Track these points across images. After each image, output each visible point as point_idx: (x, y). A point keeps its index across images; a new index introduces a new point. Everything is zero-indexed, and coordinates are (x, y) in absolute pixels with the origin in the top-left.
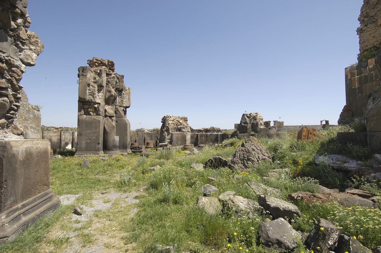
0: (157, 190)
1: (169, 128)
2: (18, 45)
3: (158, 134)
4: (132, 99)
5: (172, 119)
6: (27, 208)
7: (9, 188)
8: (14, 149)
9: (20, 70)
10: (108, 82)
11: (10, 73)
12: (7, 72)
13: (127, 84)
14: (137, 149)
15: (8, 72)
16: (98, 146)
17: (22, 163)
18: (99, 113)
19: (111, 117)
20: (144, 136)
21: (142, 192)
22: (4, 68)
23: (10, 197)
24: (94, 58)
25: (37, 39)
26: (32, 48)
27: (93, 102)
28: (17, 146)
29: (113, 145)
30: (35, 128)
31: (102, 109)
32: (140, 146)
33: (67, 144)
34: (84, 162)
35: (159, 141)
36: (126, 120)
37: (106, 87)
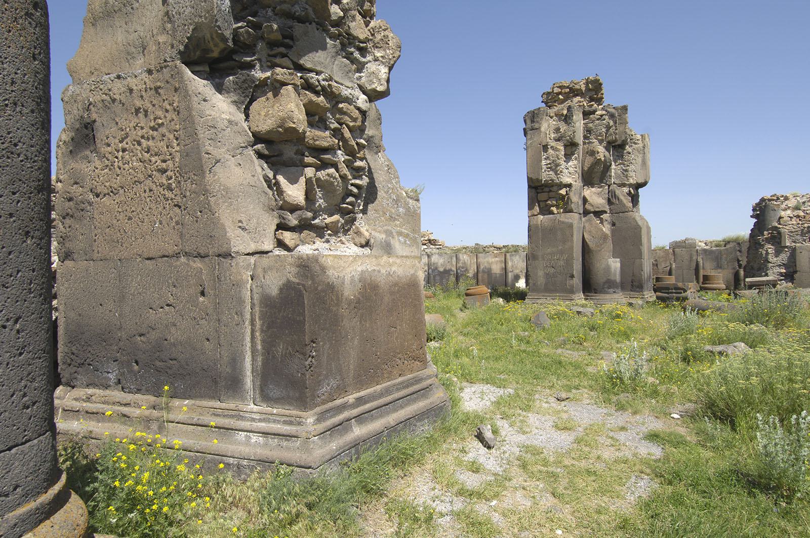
0: (734, 429)
1: (779, 233)
2: (351, 56)
3: (740, 251)
4: (651, 163)
5: (792, 203)
6: (367, 406)
7: (324, 359)
8: (330, 272)
9: (354, 106)
10: (588, 131)
11: (338, 116)
12: (332, 114)
13: (635, 126)
14: (672, 293)
15: (334, 115)
16: (571, 282)
17: (353, 305)
18: (569, 208)
19: (598, 214)
20: (694, 258)
21: (674, 421)
22: (321, 104)
23: (327, 377)
24: (555, 86)
25: (386, 33)
26: (378, 54)
27: (557, 185)
28: (339, 268)
29: (605, 279)
30: (408, 235)
31: (577, 196)
32: (680, 285)
33: (517, 278)
34: (535, 315)
35: (744, 271)
36: (638, 219)
37: (584, 143)
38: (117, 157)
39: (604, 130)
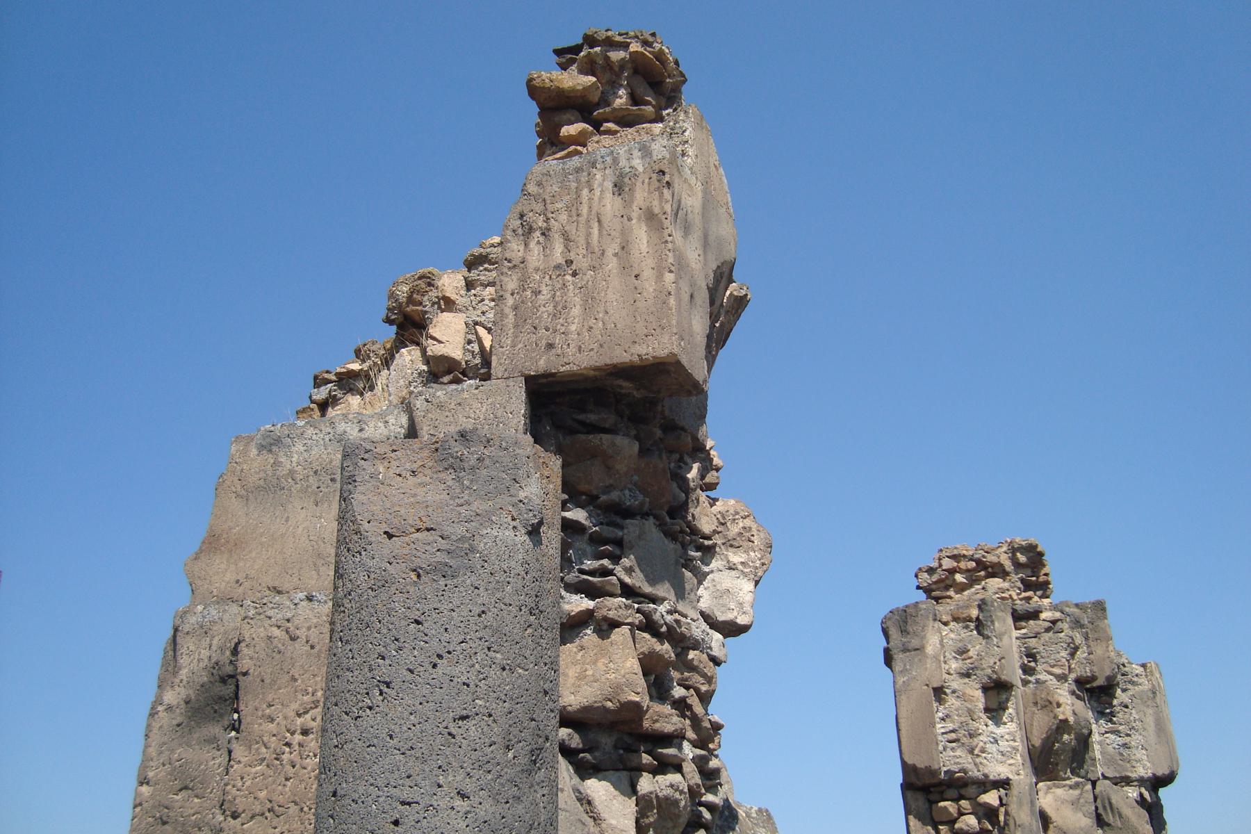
4: (1177, 729)
13: (1128, 644)
25: (748, 522)
26: (736, 558)
37: (1025, 683)
38: (288, 744)
39: (1064, 654)
